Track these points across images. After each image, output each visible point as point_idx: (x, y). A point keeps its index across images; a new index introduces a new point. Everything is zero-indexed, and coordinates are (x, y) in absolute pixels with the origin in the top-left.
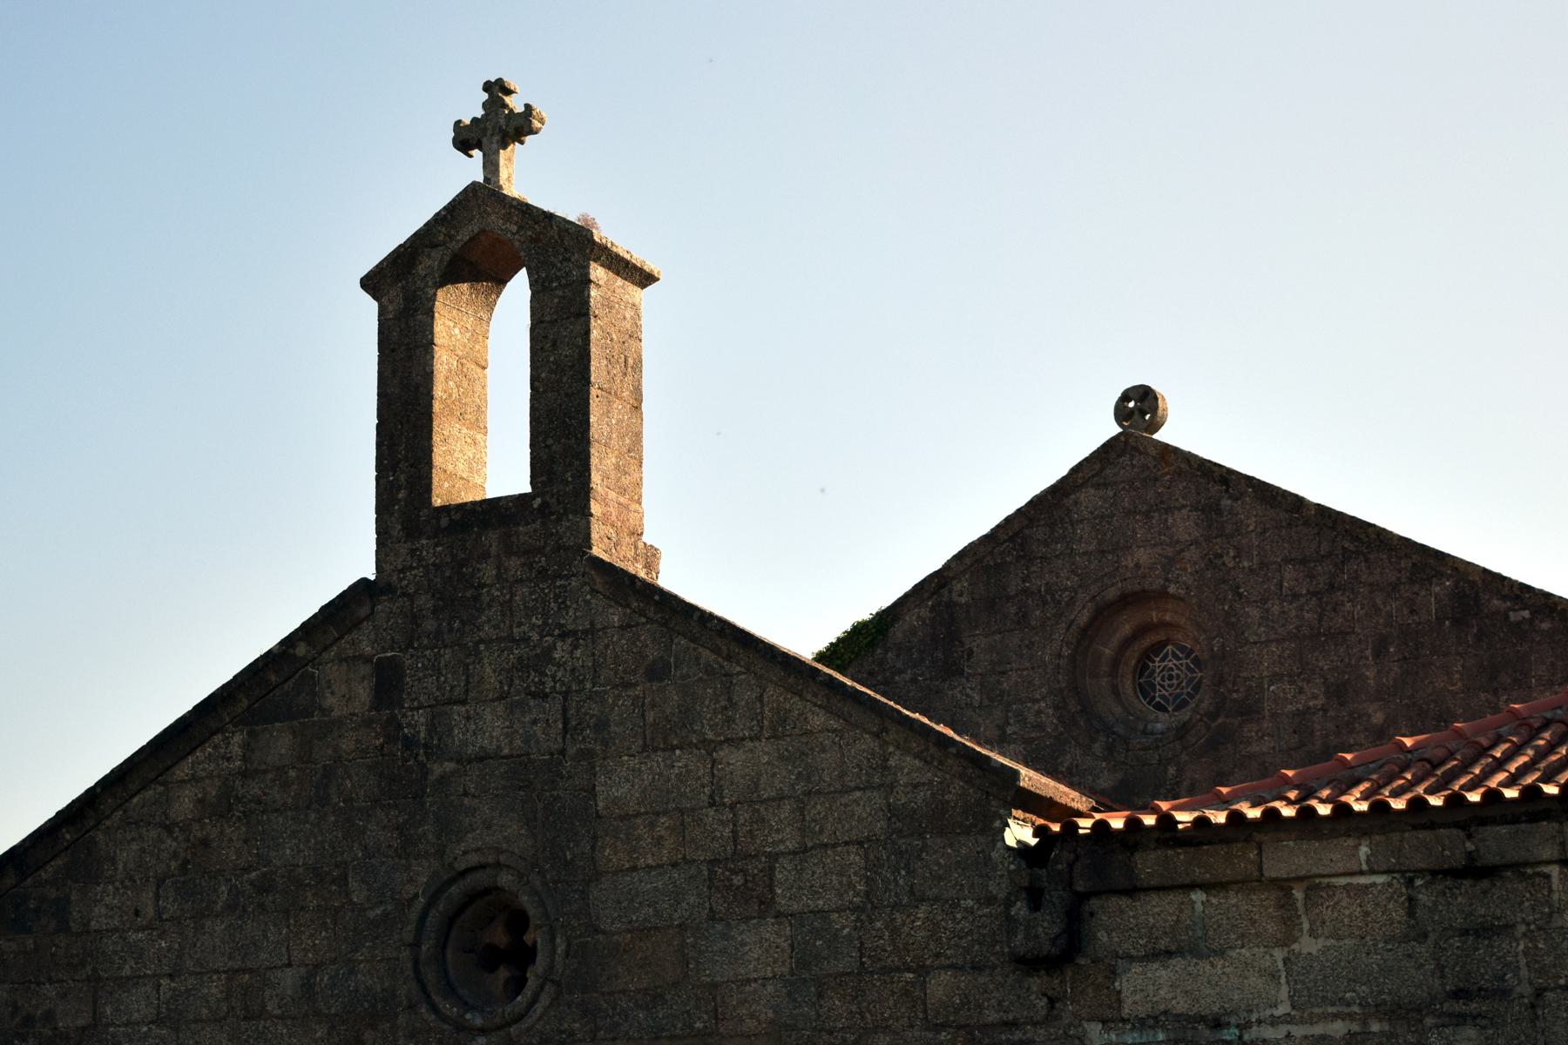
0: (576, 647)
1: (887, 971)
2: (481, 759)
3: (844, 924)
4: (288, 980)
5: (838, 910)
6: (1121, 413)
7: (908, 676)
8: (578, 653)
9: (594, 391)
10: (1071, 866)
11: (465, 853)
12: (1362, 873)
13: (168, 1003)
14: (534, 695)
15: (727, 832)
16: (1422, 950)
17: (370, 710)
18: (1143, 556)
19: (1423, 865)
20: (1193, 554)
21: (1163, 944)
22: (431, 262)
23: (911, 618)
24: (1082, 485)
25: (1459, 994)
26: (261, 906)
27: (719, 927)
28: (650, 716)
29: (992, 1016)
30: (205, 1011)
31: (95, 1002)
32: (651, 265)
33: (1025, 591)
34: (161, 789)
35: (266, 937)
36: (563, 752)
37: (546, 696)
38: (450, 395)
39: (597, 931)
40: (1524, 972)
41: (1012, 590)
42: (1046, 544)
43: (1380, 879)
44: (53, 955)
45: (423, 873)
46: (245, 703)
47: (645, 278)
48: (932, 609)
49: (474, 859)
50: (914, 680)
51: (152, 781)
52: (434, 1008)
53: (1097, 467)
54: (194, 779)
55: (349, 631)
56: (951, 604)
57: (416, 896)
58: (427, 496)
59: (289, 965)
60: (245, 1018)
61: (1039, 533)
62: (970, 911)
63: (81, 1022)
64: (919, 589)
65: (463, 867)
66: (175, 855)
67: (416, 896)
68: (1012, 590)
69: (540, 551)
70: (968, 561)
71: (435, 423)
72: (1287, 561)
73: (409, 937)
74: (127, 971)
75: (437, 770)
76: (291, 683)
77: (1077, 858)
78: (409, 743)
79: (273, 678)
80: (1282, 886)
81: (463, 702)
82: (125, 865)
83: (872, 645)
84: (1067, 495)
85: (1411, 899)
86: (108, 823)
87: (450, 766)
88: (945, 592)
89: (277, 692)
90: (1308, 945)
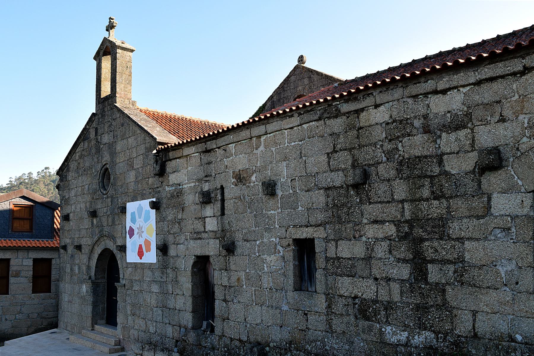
6: (299, 61)
9: (117, 73)
10: (162, 156)
12: (194, 153)
16: (202, 168)
18: (300, 88)
19: (201, 151)
20: (307, 87)
21: (174, 170)
22: (101, 53)
24: (292, 76)
25: (206, 176)
32: (132, 48)
33: (284, 97)
38: (106, 77)
40: (214, 171)
41: (282, 97)
42: (287, 88)
43: (197, 154)
46: (82, 138)
47: (132, 51)
52: (101, 191)
53: (294, 72)
54: (78, 152)
56: (274, 101)
61: (286, 86)
68: (282, 97)
70: (276, 93)
71: (102, 83)
72: (321, 86)
73: (98, 178)
77: (163, 154)
80: (187, 156)
81: (103, 134)
84: (289, 78)
85: (201, 158)
90: (189, 168)
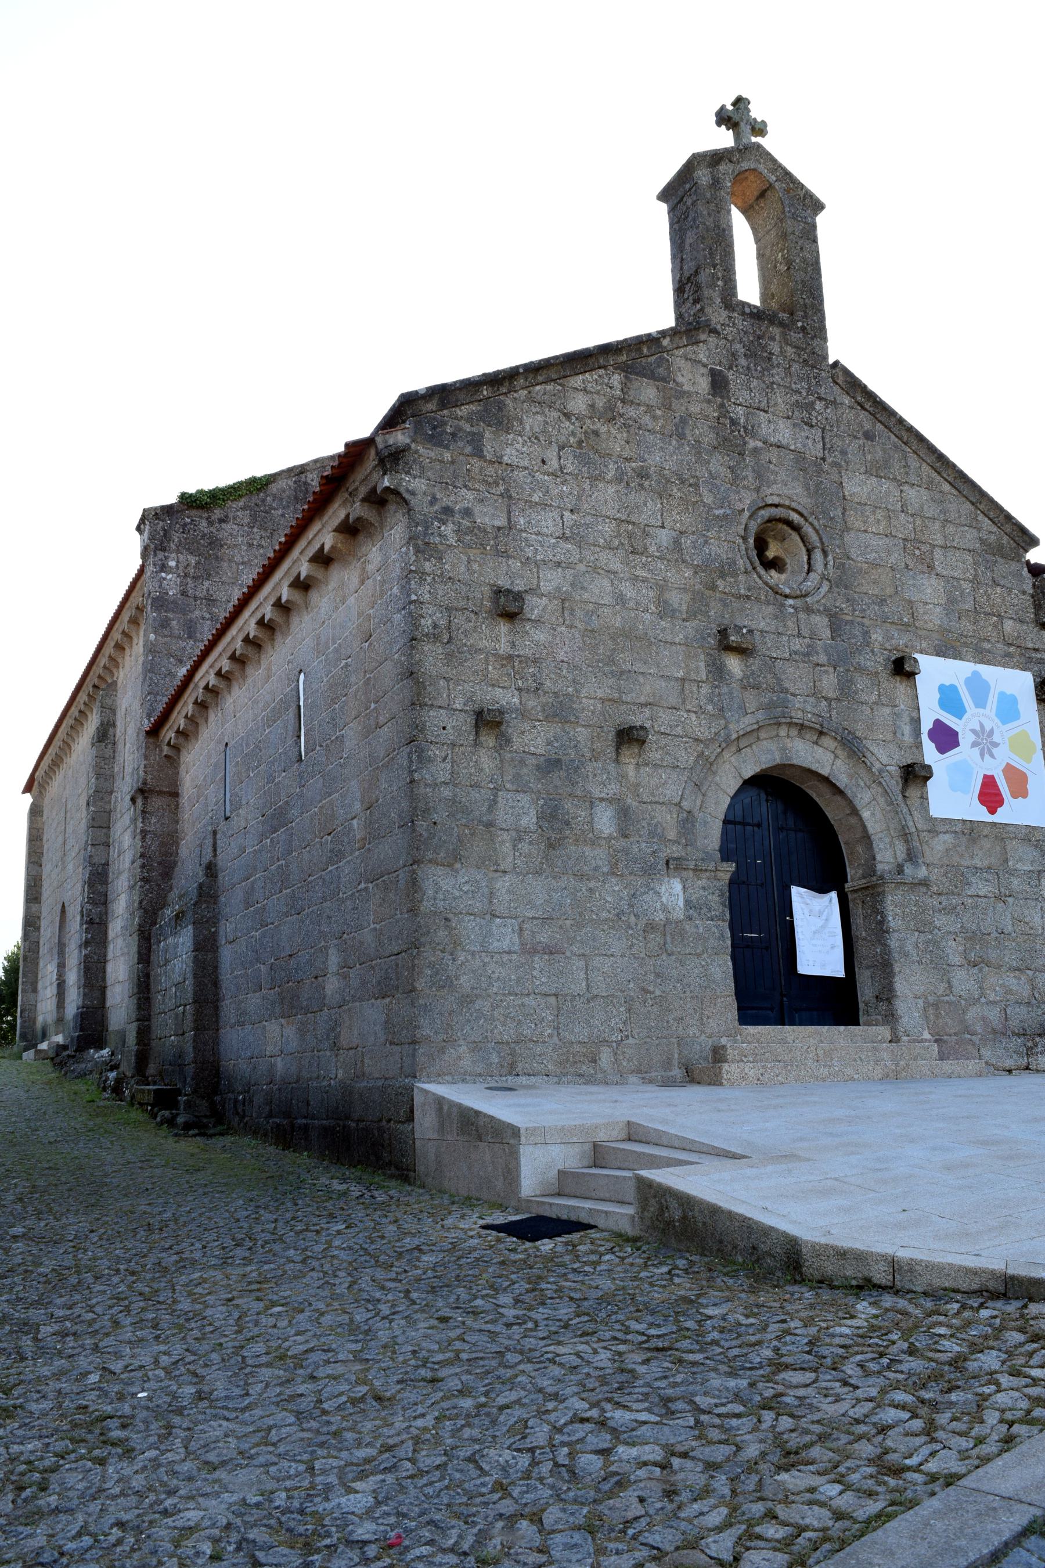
0: (827, 407)
1: (987, 614)
2: (779, 447)
3: (967, 586)
4: (664, 537)
5: (964, 580)
7: (280, 512)
8: (828, 411)
11: (771, 494)
13: (571, 528)
14: (806, 424)
15: (911, 527)
17: (709, 394)
23: (282, 484)
26: (641, 485)
27: (911, 573)
28: (869, 457)
29: (1030, 645)
30: (602, 541)
31: (509, 512)
34: (560, 388)
35: (645, 505)
36: (824, 459)
37: (812, 426)
39: (849, 558)
44: (468, 470)
45: (746, 500)
46: (624, 358)
48: (295, 482)
49: (775, 500)
50: (283, 515)
51: (552, 380)
55: (692, 344)
57: (743, 510)
58: (773, 288)
59: (663, 527)
60: (632, 552)
62: (1017, 595)
63: (498, 523)
64: (290, 470)
65: (770, 502)
66: (573, 434)
67: (743, 510)
69: (804, 349)
70: (318, 465)
74: (536, 498)
75: (752, 444)
76: (654, 358)
78: (734, 422)
79: (645, 351)
82: (531, 428)
83: (259, 490)
86: (515, 395)
87: (760, 444)
88: (303, 476)
89: (644, 360)
